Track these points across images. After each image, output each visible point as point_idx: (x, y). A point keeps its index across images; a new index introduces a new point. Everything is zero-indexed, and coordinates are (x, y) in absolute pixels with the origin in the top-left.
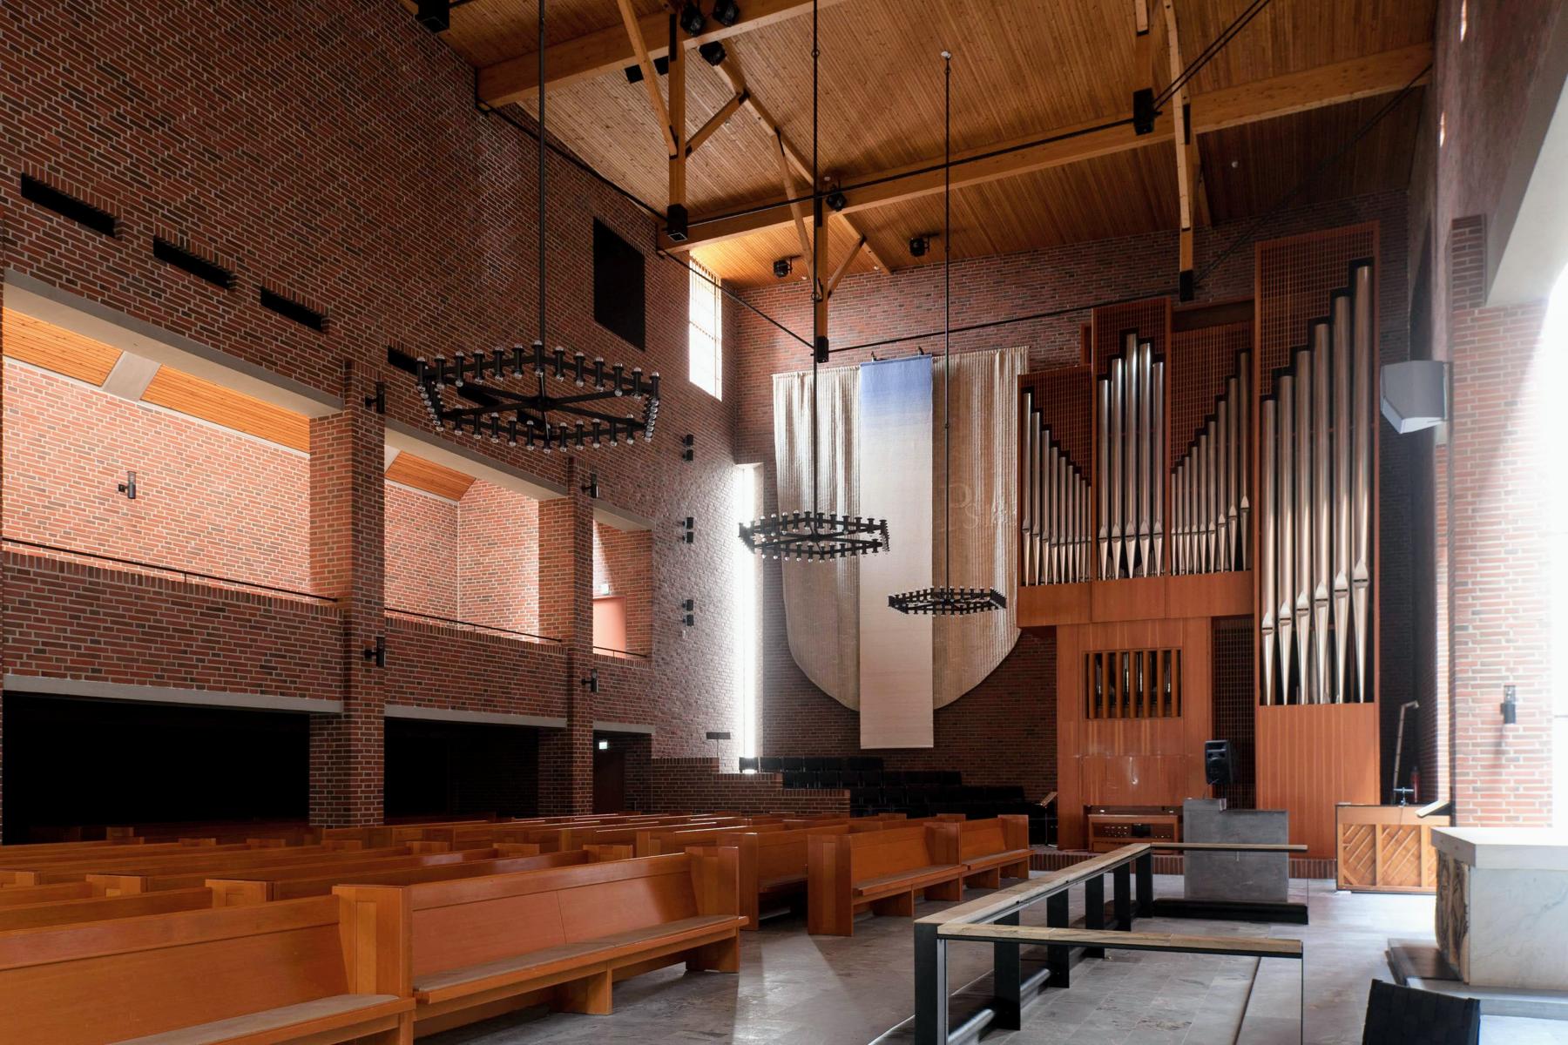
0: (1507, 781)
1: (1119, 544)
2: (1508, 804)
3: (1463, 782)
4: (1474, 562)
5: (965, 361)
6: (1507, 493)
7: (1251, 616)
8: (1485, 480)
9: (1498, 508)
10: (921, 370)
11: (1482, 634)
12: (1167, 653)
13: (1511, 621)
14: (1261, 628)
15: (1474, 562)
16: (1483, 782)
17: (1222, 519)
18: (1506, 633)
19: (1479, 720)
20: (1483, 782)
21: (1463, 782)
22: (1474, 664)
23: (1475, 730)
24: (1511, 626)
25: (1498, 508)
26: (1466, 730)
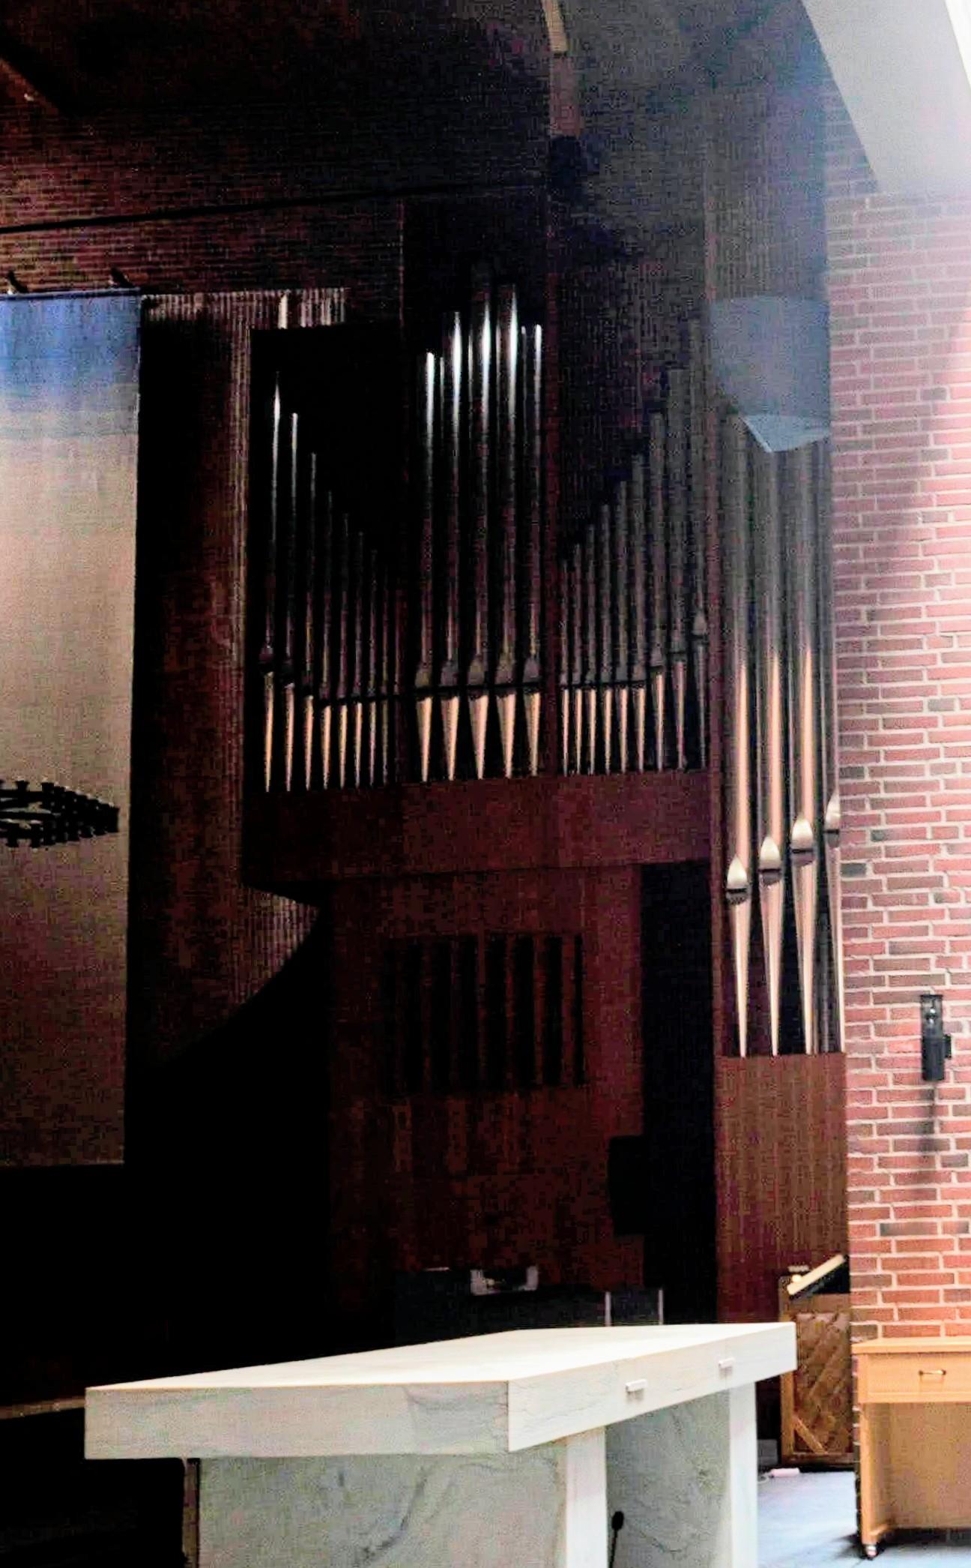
0: (946, 1211)
1: (483, 702)
2: (949, 1262)
3: (861, 1214)
4: (873, 725)
5: (217, 309)
6: (931, 580)
7: (706, 864)
8: (890, 551)
9: (916, 612)
10: (111, 317)
11: (893, 884)
12: (554, 944)
13: (944, 855)
14: (724, 889)
15: (873, 725)
16: (901, 1213)
17: (657, 658)
18: (936, 882)
19: (889, 1074)
20: (901, 1213)
21: (861, 1214)
22: (879, 948)
23: (883, 1096)
24: (944, 866)
25: (916, 612)
26: (866, 1096)
